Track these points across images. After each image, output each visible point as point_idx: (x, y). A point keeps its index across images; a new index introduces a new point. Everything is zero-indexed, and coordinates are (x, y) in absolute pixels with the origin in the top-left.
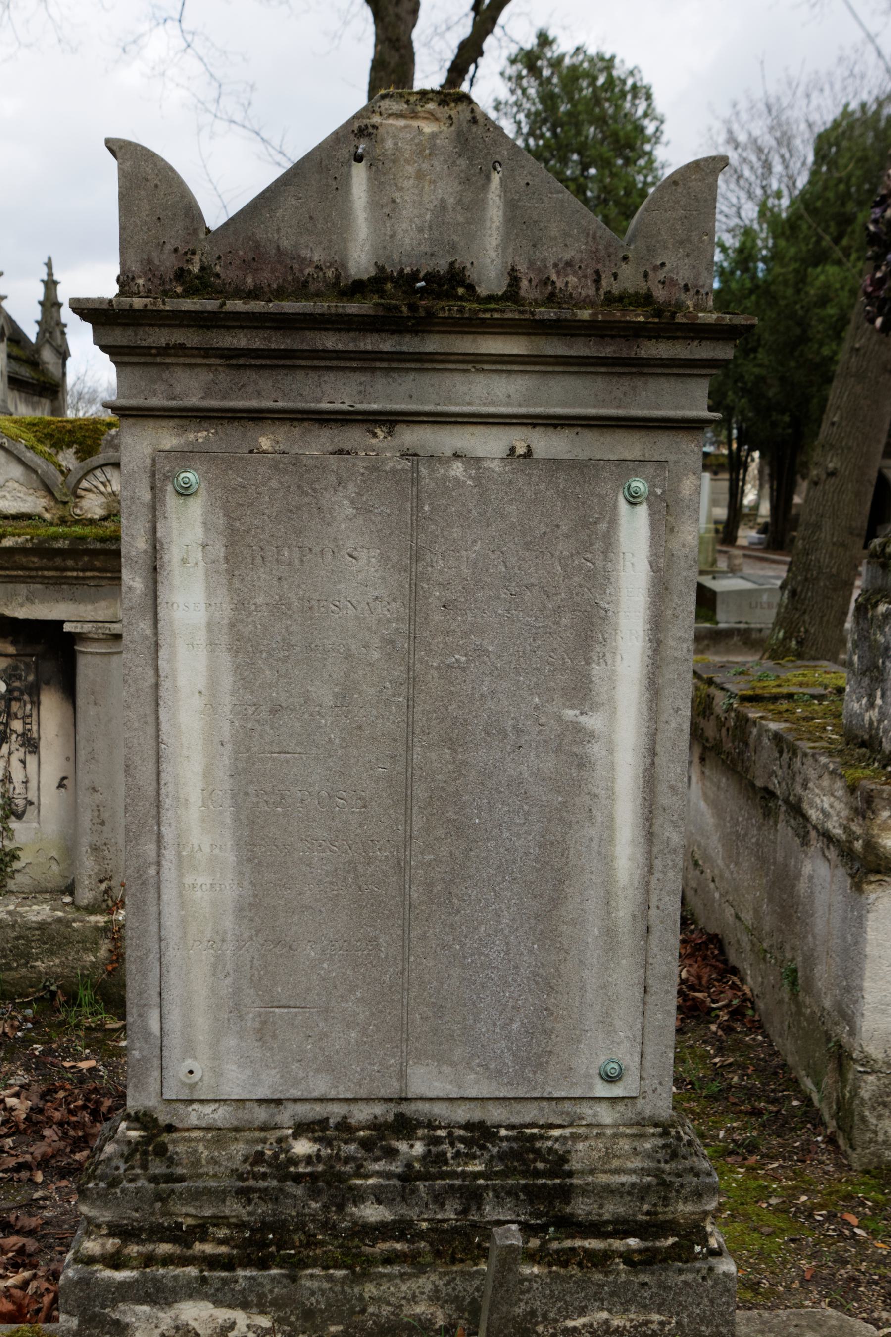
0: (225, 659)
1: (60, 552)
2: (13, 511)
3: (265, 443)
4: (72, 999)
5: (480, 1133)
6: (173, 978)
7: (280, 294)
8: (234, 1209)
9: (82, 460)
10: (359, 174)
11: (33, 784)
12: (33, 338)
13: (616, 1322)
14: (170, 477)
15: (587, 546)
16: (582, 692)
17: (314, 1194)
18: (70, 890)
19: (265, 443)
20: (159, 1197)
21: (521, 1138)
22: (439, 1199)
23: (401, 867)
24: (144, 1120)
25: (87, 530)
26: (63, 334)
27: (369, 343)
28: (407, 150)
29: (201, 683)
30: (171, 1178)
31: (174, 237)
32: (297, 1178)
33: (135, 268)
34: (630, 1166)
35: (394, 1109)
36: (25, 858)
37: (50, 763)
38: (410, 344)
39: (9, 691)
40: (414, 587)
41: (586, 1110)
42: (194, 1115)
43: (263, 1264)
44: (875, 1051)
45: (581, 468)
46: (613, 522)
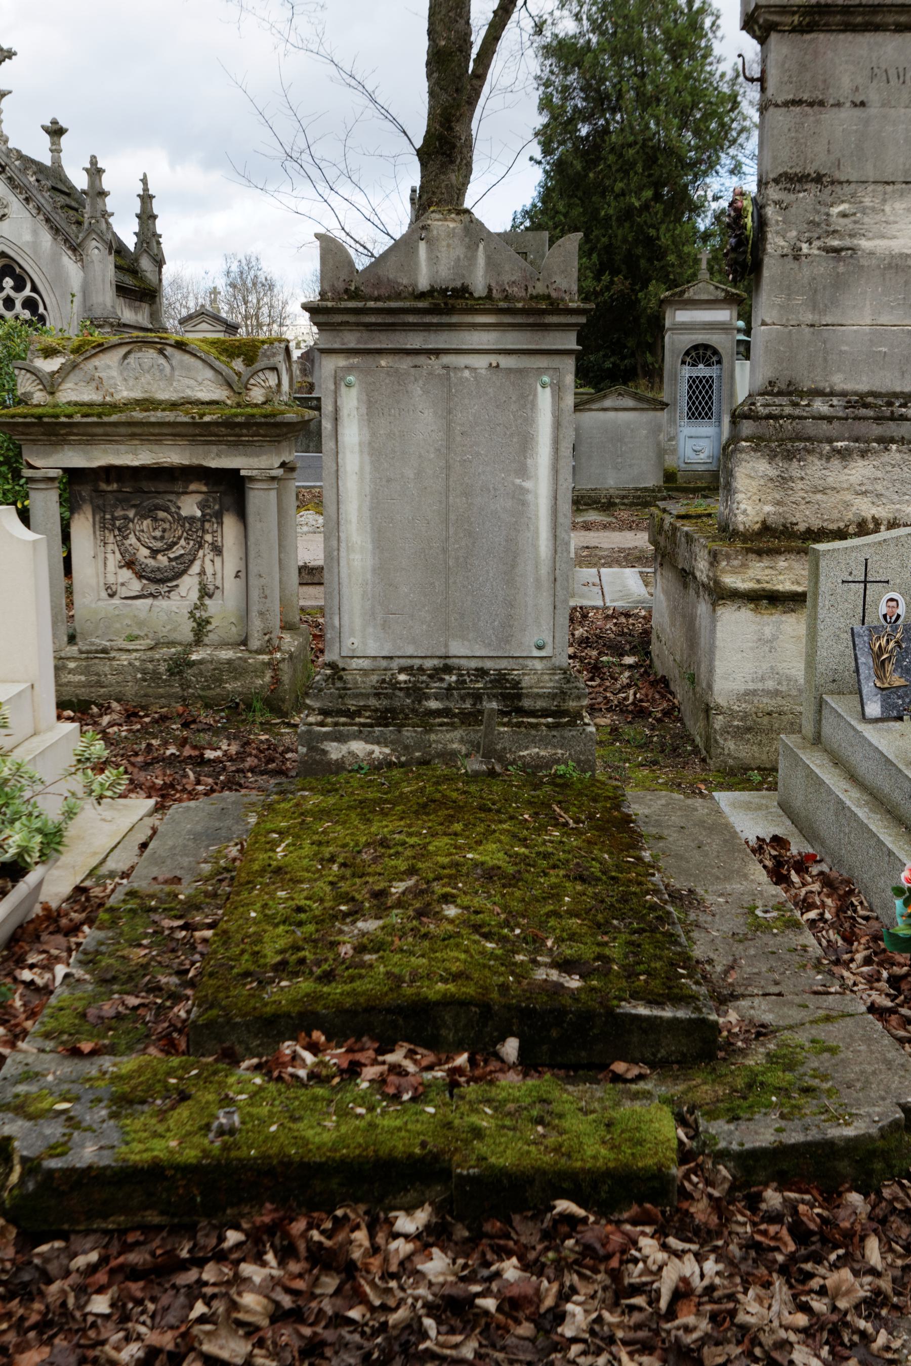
0: (367, 458)
1: (239, 425)
2: (207, 399)
3: (383, 363)
4: (249, 707)
5: (482, 673)
6: (345, 601)
7: (389, 298)
8: (373, 702)
9: (248, 365)
10: (422, 246)
11: (219, 575)
12: (132, 248)
13: (542, 753)
14: (343, 379)
15: (524, 406)
16: (523, 471)
17: (408, 695)
18: (244, 643)
19: (383, 363)
20: (341, 697)
21: (500, 674)
22: (463, 699)
23: (445, 551)
24: (332, 665)
25: (255, 411)
26: (159, 243)
27: (428, 319)
28: (443, 234)
29: (356, 469)
30: (345, 689)
31: (344, 275)
32: (401, 689)
33: (327, 288)
34: (549, 684)
35: (443, 662)
36: (215, 623)
37: (231, 560)
38: (445, 319)
39: (203, 515)
40: (449, 425)
41: (529, 663)
42: (355, 664)
43: (386, 726)
44: (722, 701)
45: (520, 371)
46: (535, 395)
